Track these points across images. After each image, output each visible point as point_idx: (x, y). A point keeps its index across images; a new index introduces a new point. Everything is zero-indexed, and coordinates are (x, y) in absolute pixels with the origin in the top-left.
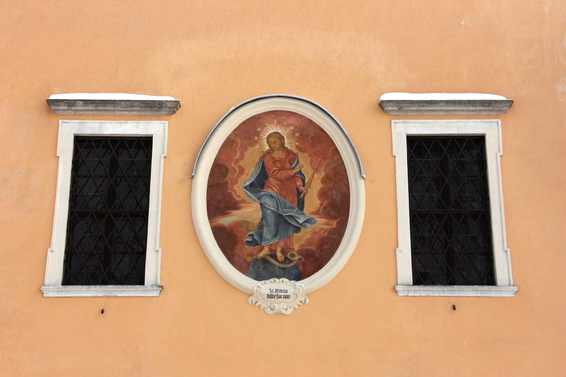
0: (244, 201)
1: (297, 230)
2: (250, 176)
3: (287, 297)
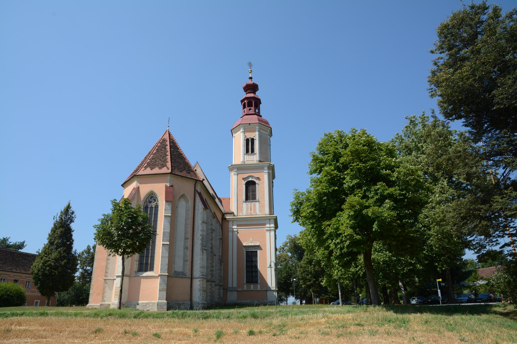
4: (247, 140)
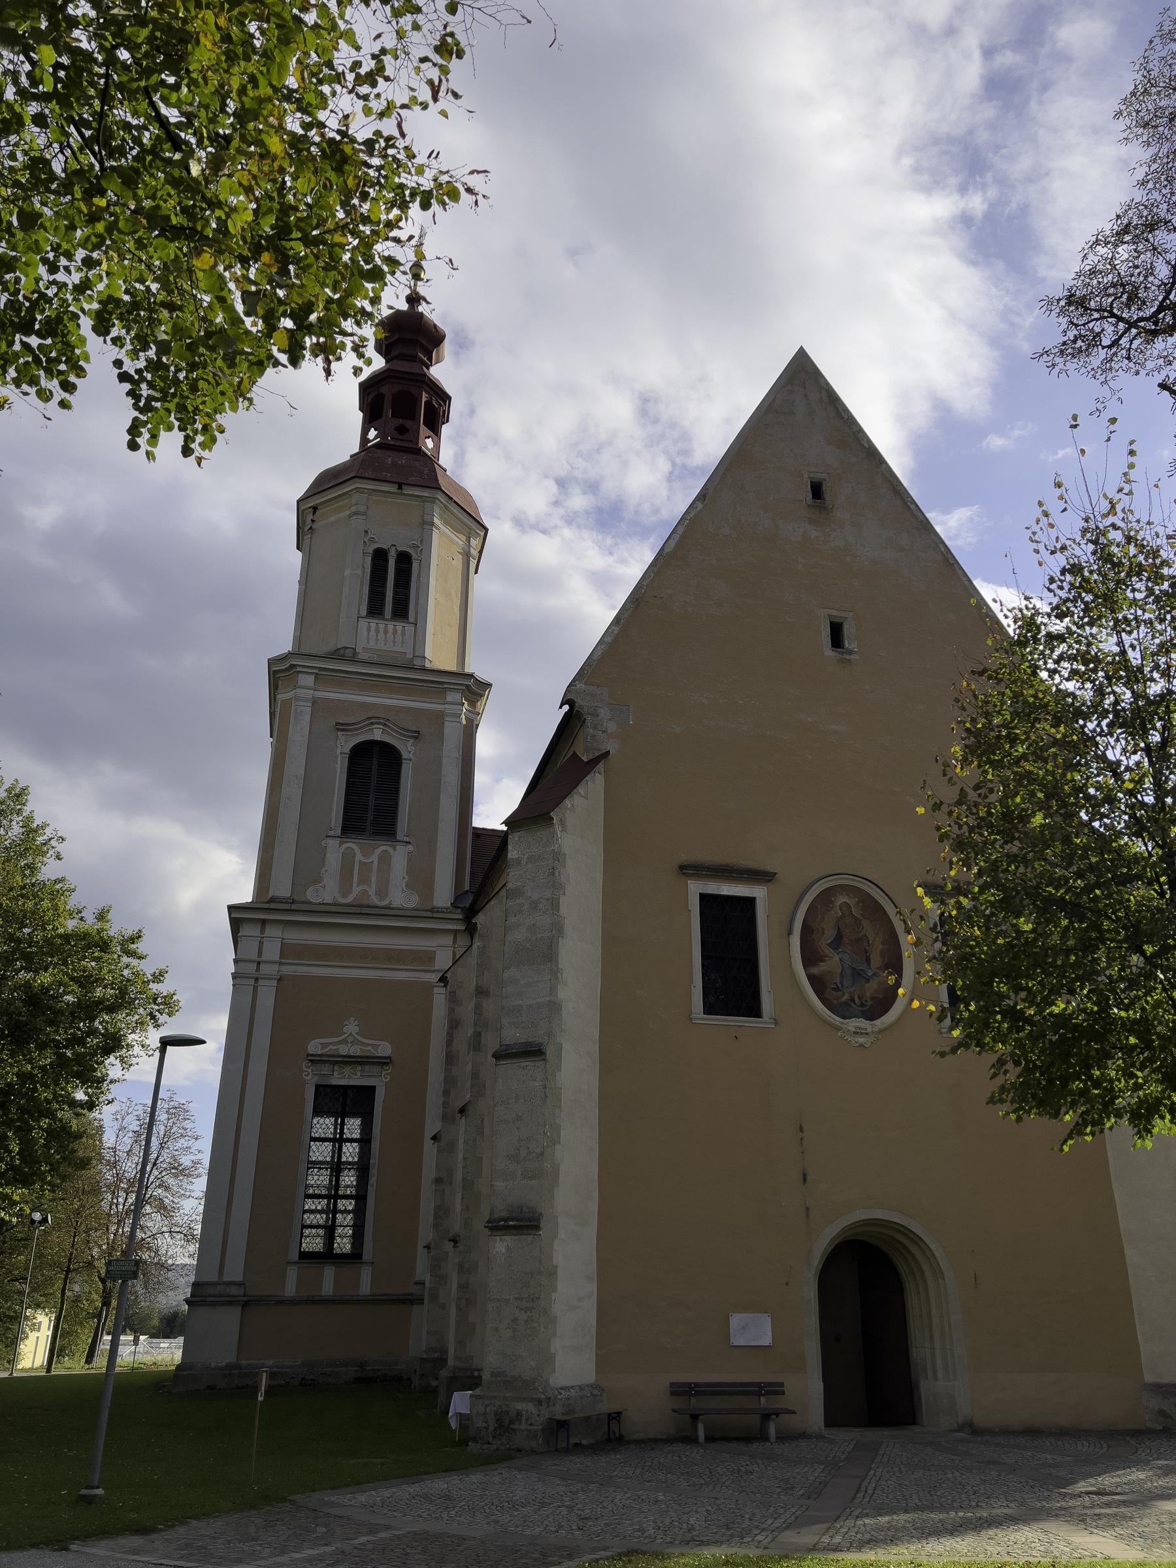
1: (868, 981)
2: (830, 934)
3: (867, 1034)
4: (380, 556)
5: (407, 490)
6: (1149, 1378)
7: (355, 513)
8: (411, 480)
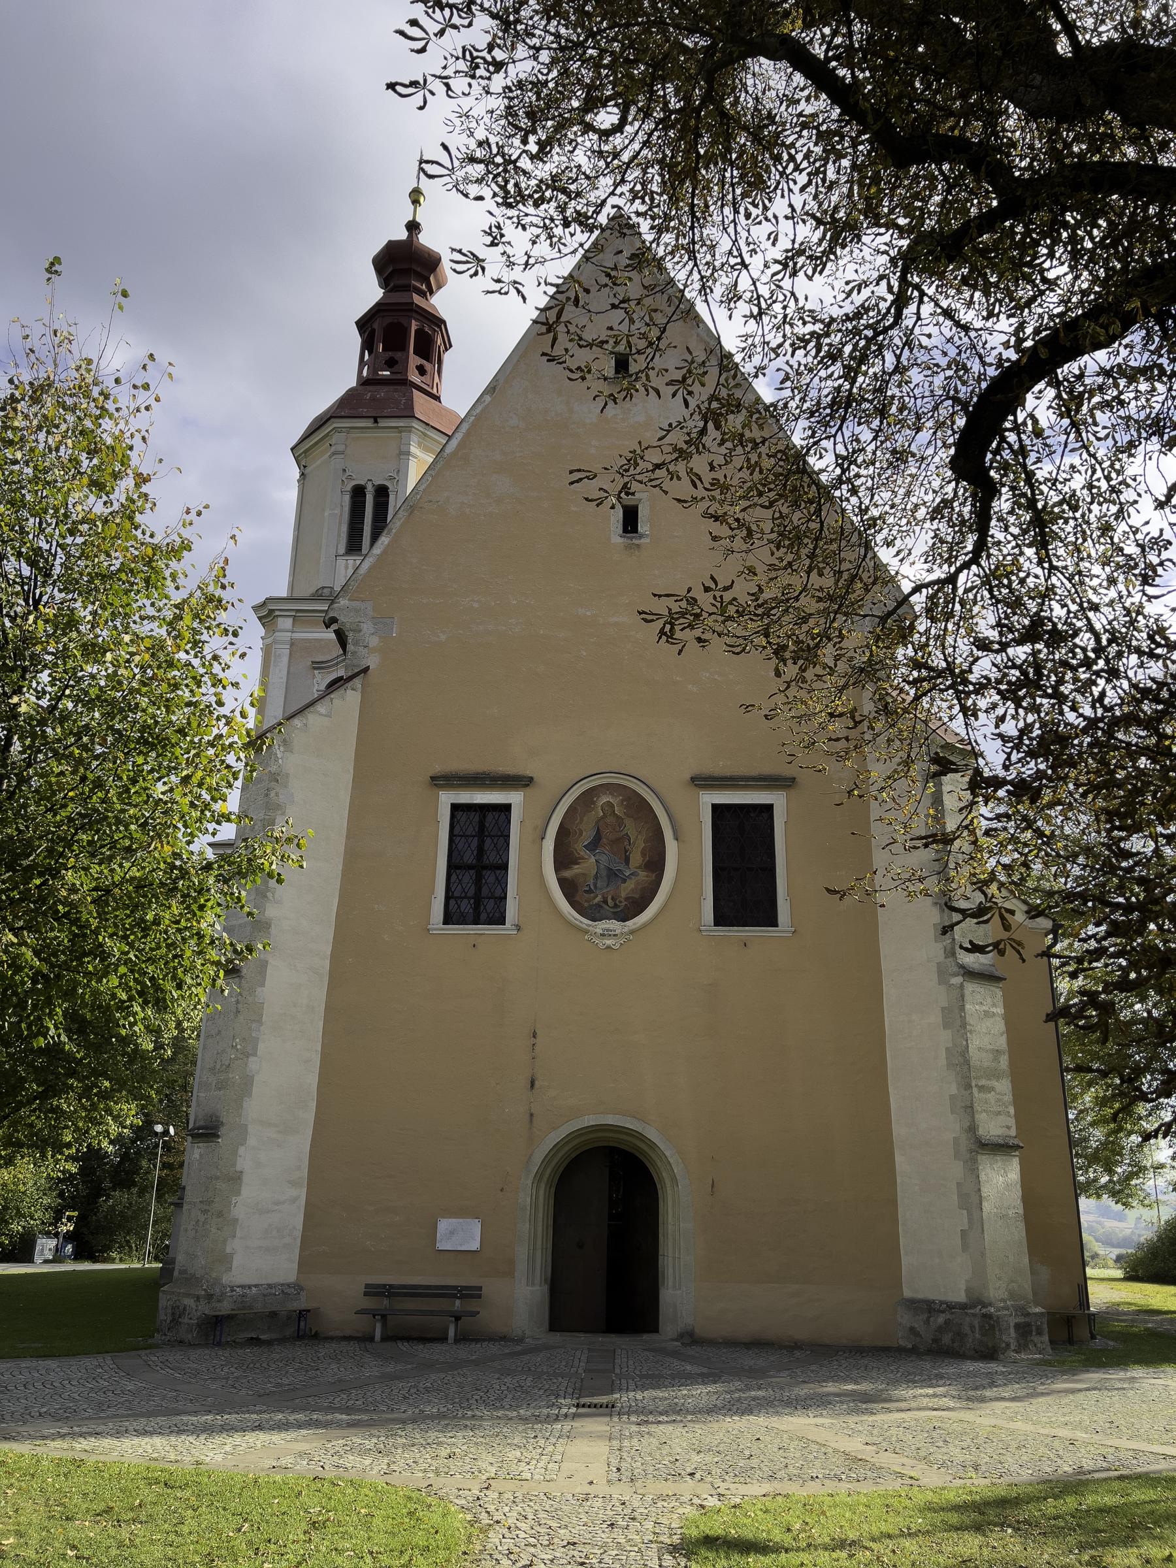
0: (583, 858)
1: (624, 881)
2: (588, 836)
4: (358, 492)
5: (383, 423)
6: (907, 1293)
7: (334, 454)
8: (386, 412)
